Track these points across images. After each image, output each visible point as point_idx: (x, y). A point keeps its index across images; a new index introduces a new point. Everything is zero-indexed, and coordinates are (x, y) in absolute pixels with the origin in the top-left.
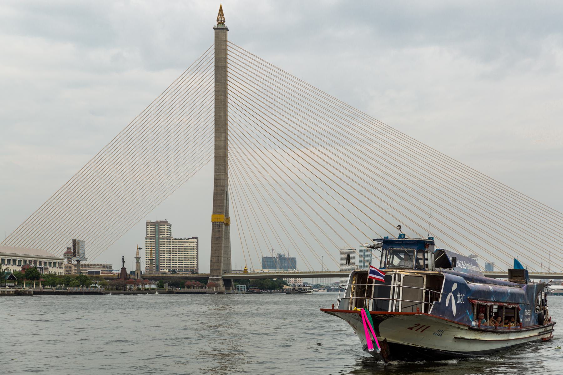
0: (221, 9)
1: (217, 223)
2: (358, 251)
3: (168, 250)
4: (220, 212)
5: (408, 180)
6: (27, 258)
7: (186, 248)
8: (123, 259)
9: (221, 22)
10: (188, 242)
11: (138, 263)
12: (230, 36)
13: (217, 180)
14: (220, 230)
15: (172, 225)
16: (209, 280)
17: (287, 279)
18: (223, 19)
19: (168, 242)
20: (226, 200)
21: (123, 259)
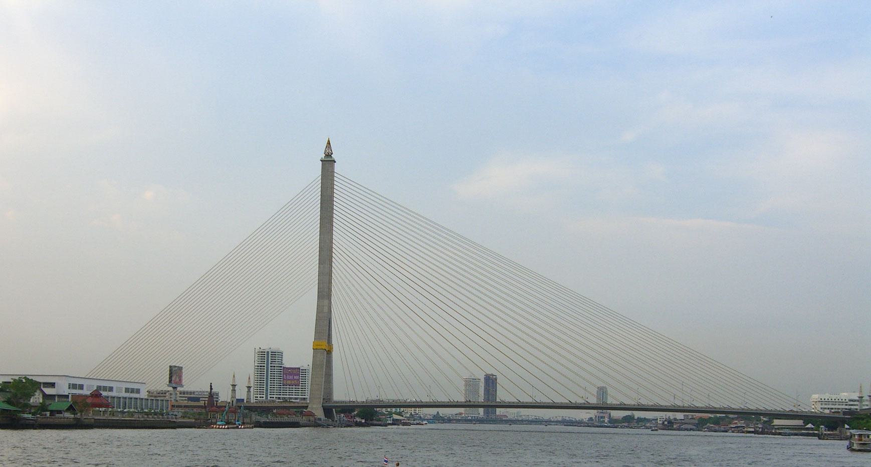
0: (329, 143)
2: (483, 380)
5: (548, 317)
8: (211, 386)
9: (328, 155)
11: (249, 391)
12: (337, 168)
15: (265, 347)
16: (818, 395)
18: (330, 151)
21: (211, 386)
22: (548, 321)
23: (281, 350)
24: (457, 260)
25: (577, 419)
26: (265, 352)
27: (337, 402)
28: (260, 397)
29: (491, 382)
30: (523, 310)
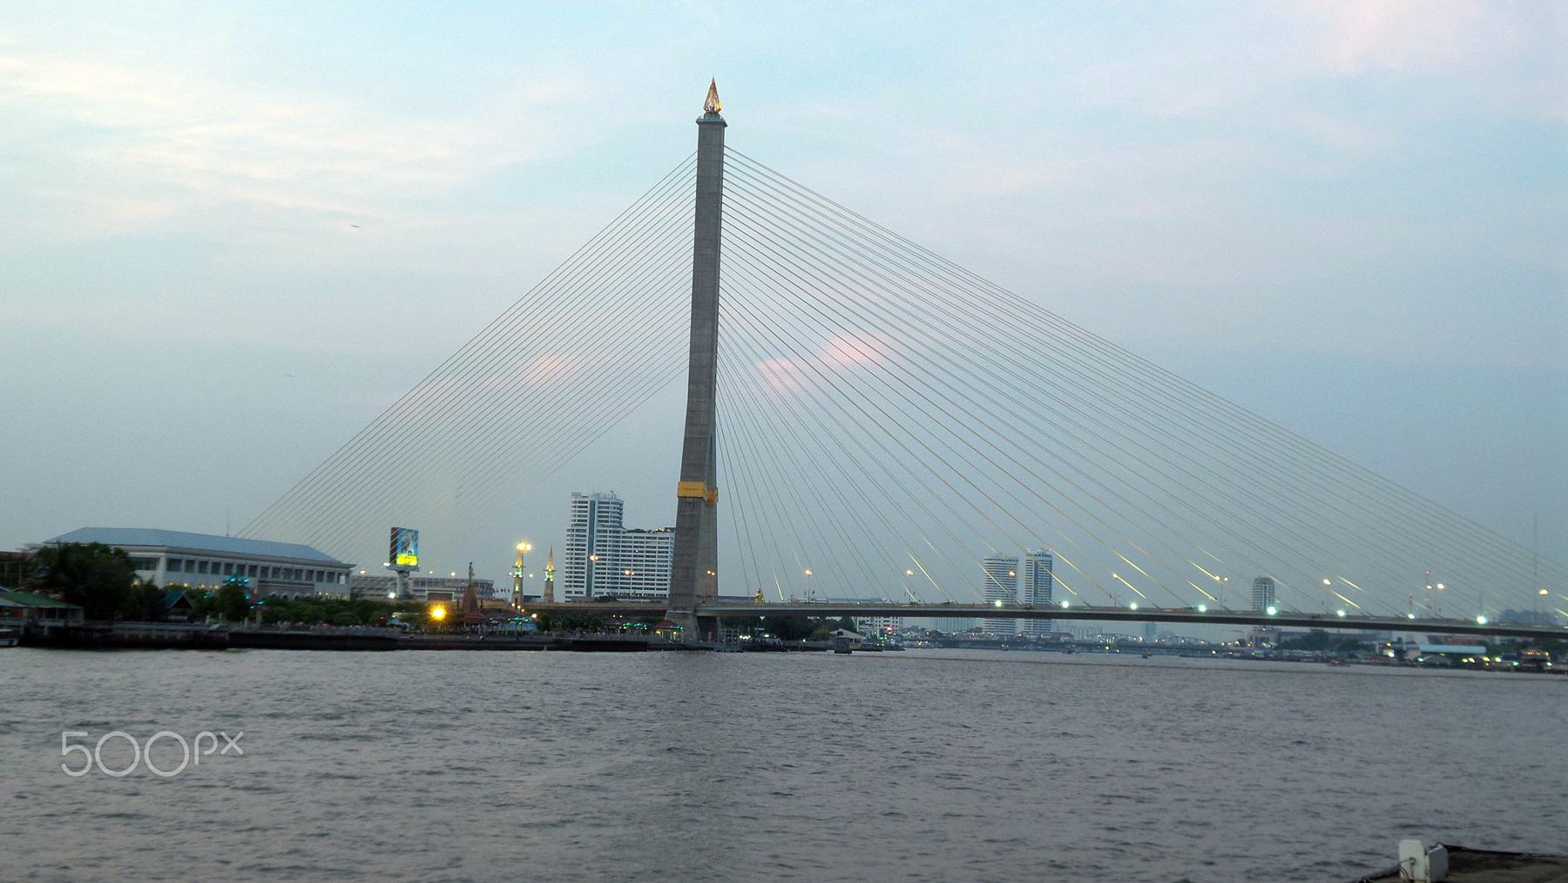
0: (713, 87)
1: (688, 500)
3: (614, 553)
4: (696, 478)
6: (180, 556)
7: (651, 551)
10: (655, 538)
12: (730, 138)
13: (692, 412)
14: (694, 513)
15: (588, 492)
17: (869, 618)
19: (614, 537)
20: (711, 453)
22: (997, 313)
23: (620, 497)
24: (935, 295)
25: (1212, 643)
26: (587, 503)
27: (770, 604)
28: (576, 593)
29: (1041, 570)
30: (957, 308)
